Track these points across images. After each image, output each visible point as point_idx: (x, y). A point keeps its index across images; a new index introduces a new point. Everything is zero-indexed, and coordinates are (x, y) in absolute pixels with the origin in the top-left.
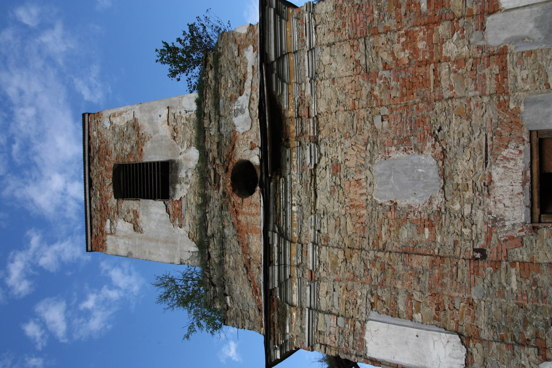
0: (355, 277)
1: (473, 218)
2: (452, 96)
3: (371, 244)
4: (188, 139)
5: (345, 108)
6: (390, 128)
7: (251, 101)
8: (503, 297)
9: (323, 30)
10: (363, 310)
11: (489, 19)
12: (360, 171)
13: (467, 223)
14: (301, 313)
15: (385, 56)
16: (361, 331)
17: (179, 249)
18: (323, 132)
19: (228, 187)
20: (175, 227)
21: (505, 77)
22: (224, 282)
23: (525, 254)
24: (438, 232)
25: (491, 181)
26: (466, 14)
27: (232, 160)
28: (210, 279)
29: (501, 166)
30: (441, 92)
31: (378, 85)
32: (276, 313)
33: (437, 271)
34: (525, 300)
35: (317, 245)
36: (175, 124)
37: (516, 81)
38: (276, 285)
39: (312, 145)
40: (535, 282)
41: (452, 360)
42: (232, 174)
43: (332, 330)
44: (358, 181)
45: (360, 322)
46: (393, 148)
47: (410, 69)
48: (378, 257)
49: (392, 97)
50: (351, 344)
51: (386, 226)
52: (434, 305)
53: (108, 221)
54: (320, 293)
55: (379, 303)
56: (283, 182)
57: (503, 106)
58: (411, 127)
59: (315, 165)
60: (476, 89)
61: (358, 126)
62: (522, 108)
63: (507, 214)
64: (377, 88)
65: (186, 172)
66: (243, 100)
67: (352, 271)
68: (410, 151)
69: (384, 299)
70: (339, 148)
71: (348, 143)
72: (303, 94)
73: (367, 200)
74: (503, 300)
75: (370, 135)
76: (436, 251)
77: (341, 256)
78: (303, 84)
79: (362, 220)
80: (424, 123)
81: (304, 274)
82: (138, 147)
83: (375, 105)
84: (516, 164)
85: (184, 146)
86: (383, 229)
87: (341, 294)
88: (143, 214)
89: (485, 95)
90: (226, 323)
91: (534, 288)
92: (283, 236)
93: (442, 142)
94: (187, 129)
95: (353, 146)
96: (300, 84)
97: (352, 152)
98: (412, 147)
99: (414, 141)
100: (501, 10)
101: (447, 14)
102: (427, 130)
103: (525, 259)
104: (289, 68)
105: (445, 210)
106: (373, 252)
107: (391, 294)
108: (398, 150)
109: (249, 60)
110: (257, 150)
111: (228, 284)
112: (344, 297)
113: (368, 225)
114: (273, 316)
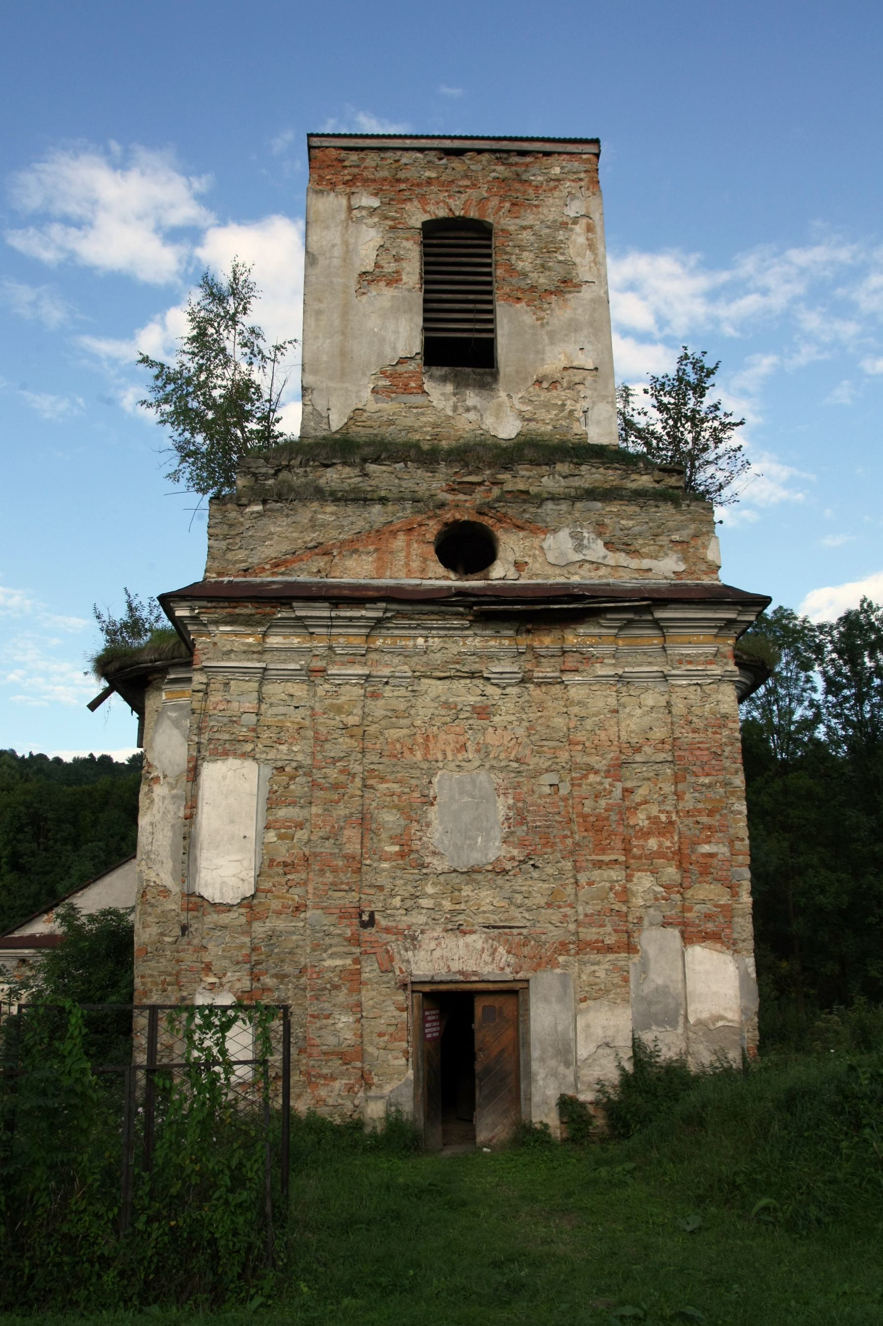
0: (321, 743)
2: (580, 884)
3: (372, 766)
4: (535, 414)
5: (572, 730)
7: (595, 565)
8: (313, 950)
9: (693, 697)
10: (272, 755)
11: (676, 932)
12: (478, 751)
13: (409, 903)
14: (254, 652)
15: (642, 792)
16: (239, 752)
17: (332, 385)
18: (538, 691)
19: (453, 515)
20: (373, 377)
21: (599, 951)
22: (286, 500)
23: (371, 975)
24: (394, 863)
25: (465, 933)
26: (686, 904)
27: (498, 525)
28: (287, 466)
29: (485, 945)
30: (585, 869)
31: (603, 780)
32: (253, 611)
33: (341, 863)
34: (311, 975)
35: (366, 681)
36: (565, 385)
37: (593, 964)
39: (520, 676)
40: (336, 987)
41: (218, 886)
42: (475, 523)
43: (235, 705)
44: (464, 747)
45: (253, 750)
46: (511, 801)
47: (621, 826)
48: (354, 777)
49: (584, 801)
50: (217, 736)
51: (399, 790)
52: (292, 859)
53: (375, 202)
54: (290, 684)
56: (462, 624)
57: (563, 949)
58: (540, 827)
59: (488, 679)
60: (586, 915)
61: (545, 749)
62: (558, 971)
63: (423, 953)
65: (475, 408)
66: (597, 550)
67: (329, 738)
68: (506, 825)
69: (292, 787)
70: (513, 718)
71: (521, 732)
72: (599, 660)
73: (437, 761)
74: (308, 950)
75: (531, 767)
76: (368, 862)
77: (352, 720)
78: (613, 661)
79: (407, 753)
80: (545, 845)
81: (319, 658)
82: (524, 291)
83: (574, 775)
84: (486, 963)
85: (523, 403)
86: (395, 786)
87: (292, 719)
89: (579, 926)
90: (214, 501)
91: (328, 986)
92: (379, 623)
93: (517, 870)
94: (554, 412)
95: (515, 740)
96: (614, 657)
97: (507, 738)
98: (512, 829)
99: (521, 831)
100: (685, 946)
101: (690, 880)
102: (535, 849)
103: (365, 976)
104: (641, 636)
105: (426, 874)
106: (361, 770)
107: (301, 798)
108: (509, 808)
109: (661, 563)
110: (513, 575)
111: (285, 508)
112: (289, 724)
113: (399, 763)
114: (247, 607)
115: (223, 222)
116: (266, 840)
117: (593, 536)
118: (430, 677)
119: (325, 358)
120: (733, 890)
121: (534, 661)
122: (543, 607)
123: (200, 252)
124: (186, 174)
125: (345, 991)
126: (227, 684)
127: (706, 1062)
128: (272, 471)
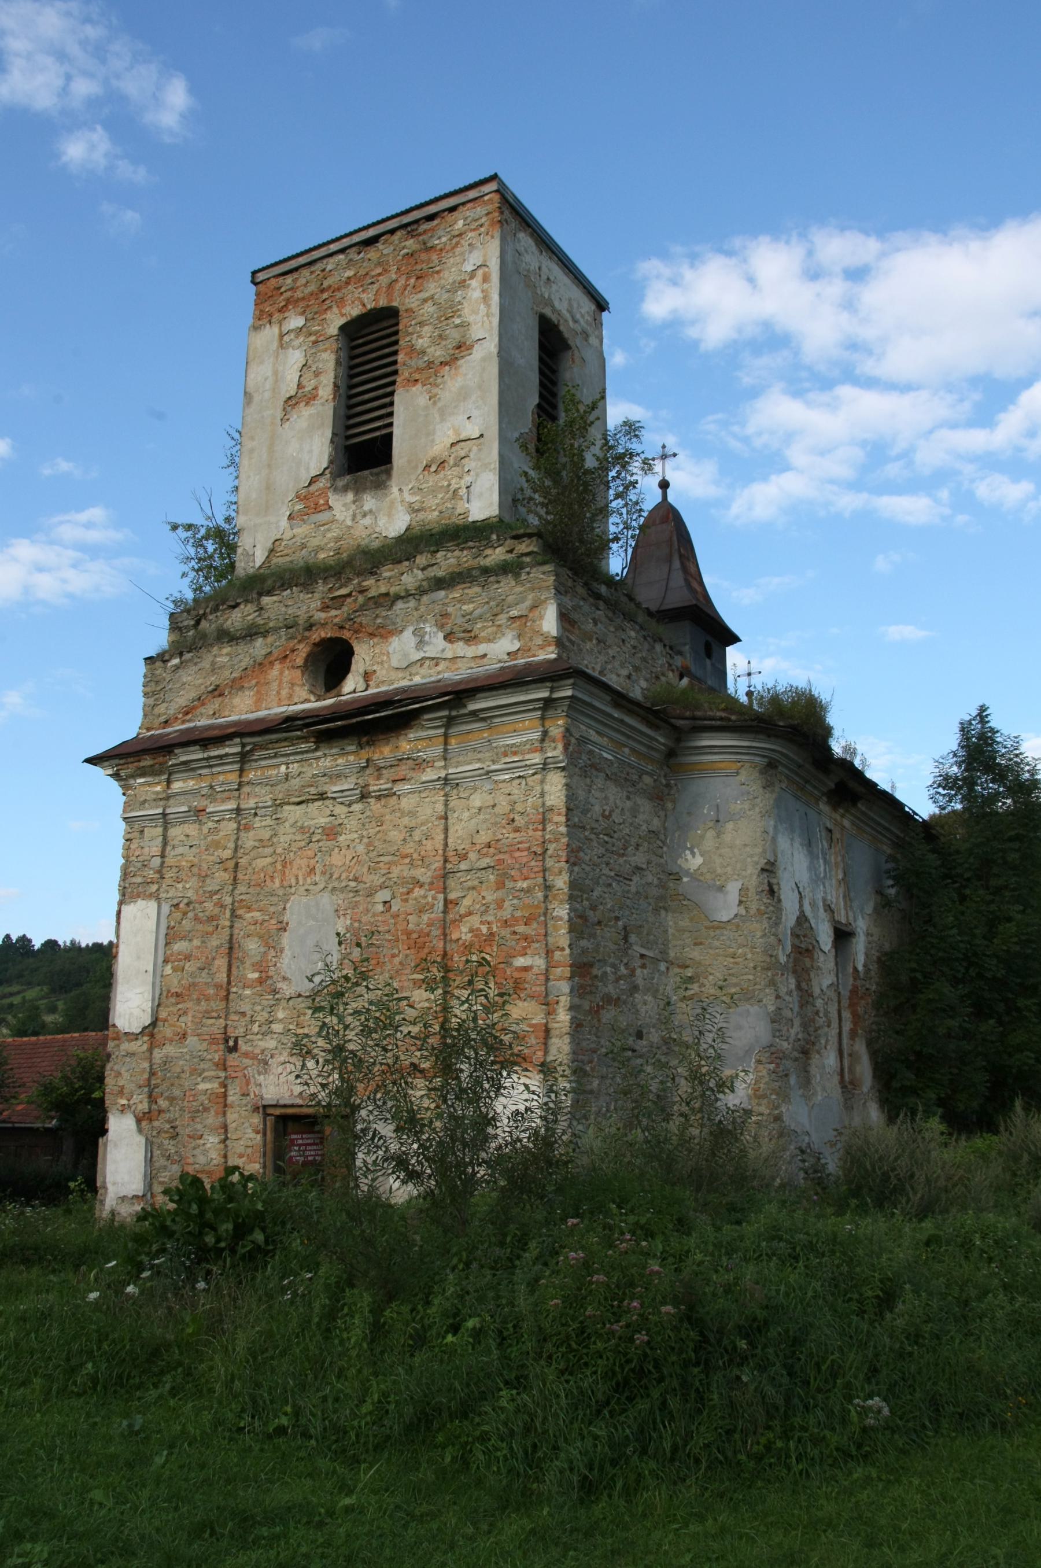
1: (270, 1035)
3: (242, 897)
6: (374, 915)
8: (191, 1074)
9: (516, 792)
13: (264, 1028)
14: (161, 799)
33: (212, 992)
38: (183, 759)
39: (358, 792)
40: (206, 1109)
41: (127, 1017)
43: (146, 850)
44: (312, 870)
45: (158, 890)
55: (178, 915)
59: (334, 798)
61: (381, 865)
63: (272, 1077)
66: (437, 645)
70: (355, 836)
71: (361, 849)
73: (291, 887)
86: (258, 914)
88: (310, 415)
92: (244, 758)
104: (470, 732)
112: (184, 863)
116: (165, 973)
117: (435, 629)
118: (289, 804)
119: (254, 496)
120: (549, 1005)
121: (376, 773)
122: (359, 719)
125: (213, 1112)
126: (142, 832)
127: (381, 1189)
128: (192, 623)
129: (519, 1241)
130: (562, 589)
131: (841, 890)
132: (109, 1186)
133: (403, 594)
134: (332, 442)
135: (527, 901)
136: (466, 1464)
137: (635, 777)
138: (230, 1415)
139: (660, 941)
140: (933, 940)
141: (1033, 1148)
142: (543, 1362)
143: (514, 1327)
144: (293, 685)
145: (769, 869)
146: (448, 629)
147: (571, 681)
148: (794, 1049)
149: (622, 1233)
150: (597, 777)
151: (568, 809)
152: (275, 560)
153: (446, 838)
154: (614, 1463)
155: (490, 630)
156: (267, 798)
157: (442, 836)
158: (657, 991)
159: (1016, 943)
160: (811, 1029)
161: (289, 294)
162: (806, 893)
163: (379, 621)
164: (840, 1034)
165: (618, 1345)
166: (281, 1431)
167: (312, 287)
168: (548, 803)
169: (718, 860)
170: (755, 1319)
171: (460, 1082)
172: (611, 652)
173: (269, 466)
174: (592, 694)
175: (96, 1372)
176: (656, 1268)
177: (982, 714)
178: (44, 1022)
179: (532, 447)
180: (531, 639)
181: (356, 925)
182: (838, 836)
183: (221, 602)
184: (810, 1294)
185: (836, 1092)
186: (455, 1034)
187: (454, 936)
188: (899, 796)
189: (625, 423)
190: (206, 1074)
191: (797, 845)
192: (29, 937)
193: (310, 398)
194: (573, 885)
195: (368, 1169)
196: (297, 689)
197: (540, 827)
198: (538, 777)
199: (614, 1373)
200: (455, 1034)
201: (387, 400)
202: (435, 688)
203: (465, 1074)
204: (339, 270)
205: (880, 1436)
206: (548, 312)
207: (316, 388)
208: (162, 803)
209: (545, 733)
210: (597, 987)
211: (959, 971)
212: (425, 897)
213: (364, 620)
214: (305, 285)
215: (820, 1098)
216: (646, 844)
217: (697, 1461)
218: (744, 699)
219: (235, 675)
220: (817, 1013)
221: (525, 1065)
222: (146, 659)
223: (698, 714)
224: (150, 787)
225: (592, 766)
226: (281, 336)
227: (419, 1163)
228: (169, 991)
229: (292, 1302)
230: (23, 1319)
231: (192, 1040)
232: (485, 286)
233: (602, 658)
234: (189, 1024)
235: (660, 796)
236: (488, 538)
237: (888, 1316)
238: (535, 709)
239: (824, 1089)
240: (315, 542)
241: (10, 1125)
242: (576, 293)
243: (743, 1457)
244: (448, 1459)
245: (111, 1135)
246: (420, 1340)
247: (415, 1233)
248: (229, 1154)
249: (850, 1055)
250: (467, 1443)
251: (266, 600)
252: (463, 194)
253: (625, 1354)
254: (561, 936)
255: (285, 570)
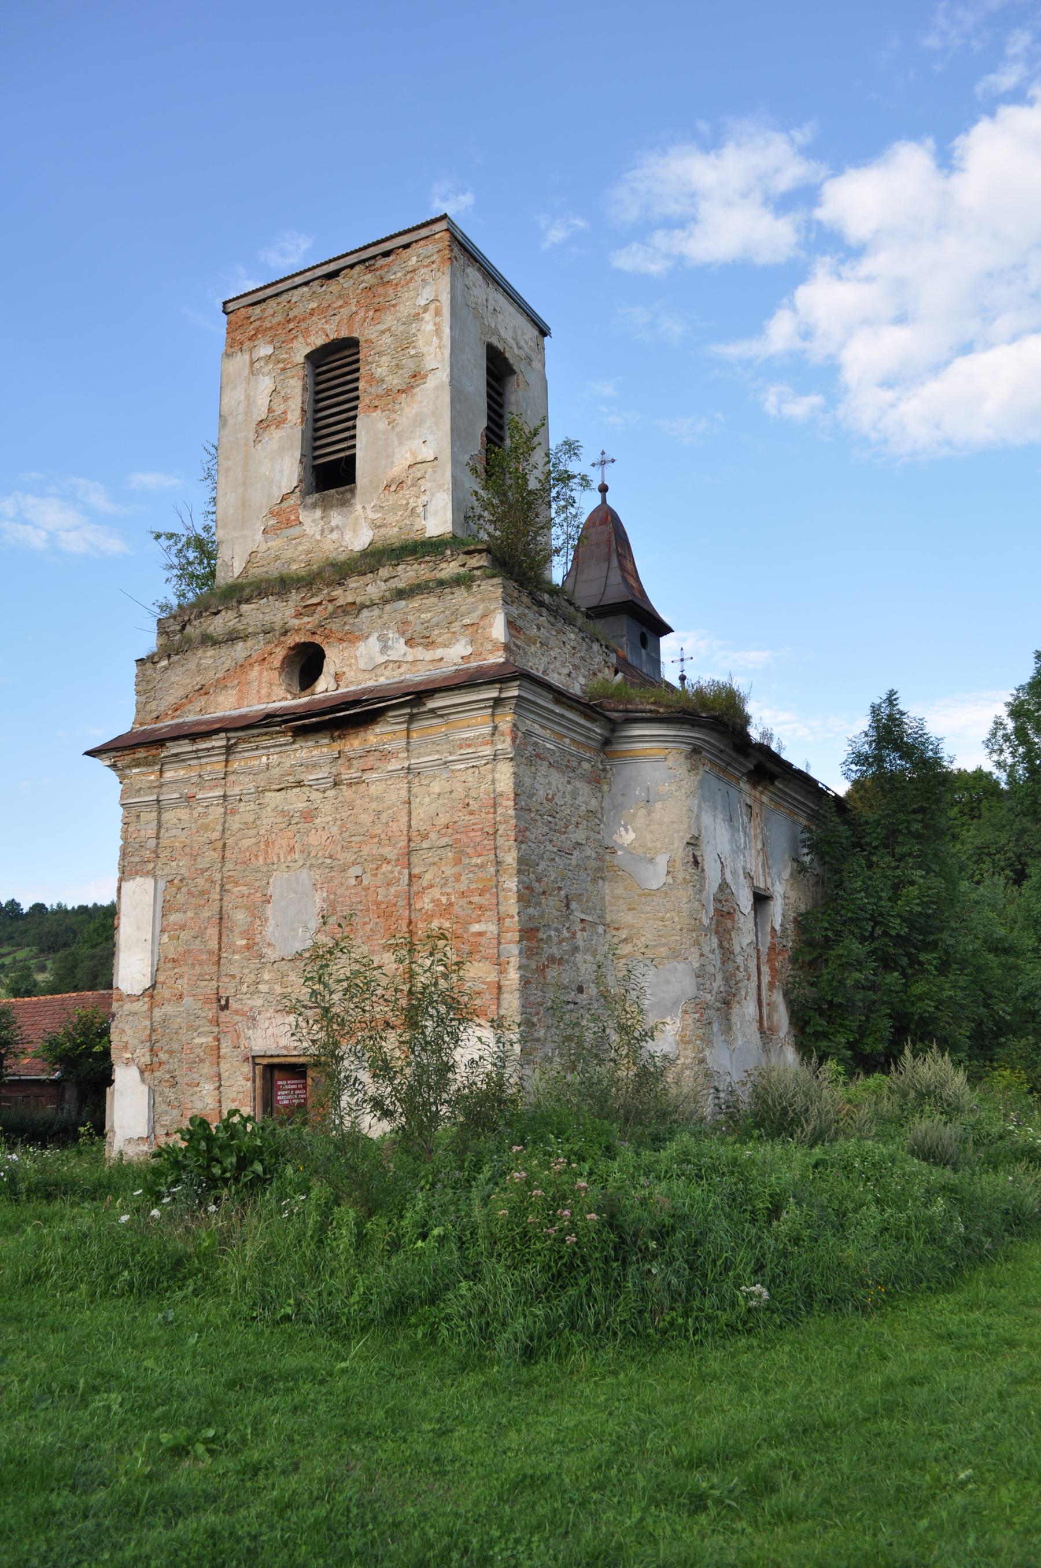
3: (230, 873)
8: (188, 1031)
9: (471, 779)
13: (252, 988)
32: (145, 755)
38: (174, 751)
39: (331, 780)
40: (202, 1061)
43: (143, 832)
44: (292, 849)
45: (154, 868)
59: (311, 786)
61: (353, 844)
64: (389, 868)
66: (399, 649)
70: (330, 818)
71: (335, 830)
86: (245, 888)
88: (280, 438)
112: (177, 844)
115: (838, 171)
117: (397, 636)
119: (231, 511)
120: (500, 965)
122: (331, 716)
123: (819, 214)
124: (785, 128)
125: (208, 1064)
128: (179, 628)
129: (475, 1166)
130: (509, 600)
131: (761, 858)
132: (116, 1129)
133: (368, 603)
134: (301, 462)
135: (481, 875)
136: (434, 1340)
137: (575, 764)
138: (245, 1308)
139: (598, 907)
140: (842, 903)
141: (919, 1086)
142: (494, 1260)
143: (471, 1233)
144: (271, 684)
145: (694, 843)
146: (408, 635)
147: (517, 683)
148: (716, 1001)
149: (558, 1157)
150: (541, 765)
151: (516, 795)
152: (252, 571)
153: (410, 820)
154: (550, 1336)
155: (445, 636)
156: (251, 785)
157: (406, 819)
158: (596, 950)
159: (918, 904)
160: (732, 983)
161: (258, 323)
162: (728, 863)
163: (347, 627)
164: (759, 987)
165: (552, 1245)
166: (287, 1318)
167: (279, 318)
168: (498, 790)
169: (649, 836)
170: (664, 1226)
171: (425, 1036)
172: (552, 653)
173: (244, 484)
174: (535, 693)
175: (132, 1278)
176: (584, 1184)
177: (891, 699)
178: (35, 981)
179: (480, 468)
180: (482, 645)
181: (332, 897)
182: (758, 811)
183: (203, 608)
184: (710, 1205)
185: (756, 1038)
186: (419, 996)
187: (418, 906)
188: (813, 774)
189: (565, 443)
190: (201, 1029)
191: (719, 820)
192: (17, 901)
193: (280, 422)
194: (521, 861)
195: (351, 1109)
196: (275, 688)
197: (492, 810)
198: (489, 766)
199: (550, 1267)
200: (419, 996)
201: (350, 424)
202: (398, 688)
203: (430, 1029)
204: (303, 300)
205: (761, 1315)
206: (494, 341)
207: (285, 412)
208: (155, 790)
209: (495, 728)
210: (543, 949)
211: (866, 930)
212: (392, 872)
213: (334, 627)
214: (273, 315)
215: (740, 1043)
216: (585, 822)
217: (615, 1334)
218: (677, 683)
219: (219, 675)
220: (738, 968)
221: (478, 1021)
222: (137, 661)
223: (630, 707)
224: (144, 776)
225: (537, 756)
226: (252, 363)
227: (393, 1103)
228: (166, 957)
229: (289, 1219)
230: (66, 1238)
231: (188, 1000)
232: (438, 319)
233: (545, 659)
234: (185, 986)
235: (597, 780)
236: (443, 553)
237: (775, 1223)
238: (486, 707)
239: (744, 1035)
240: (287, 555)
241: (17, 1078)
242: (522, 321)
243: (651, 1331)
244: (420, 1336)
245: (117, 1085)
246: (395, 1245)
247: (389, 1162)
248: (223, 1099)
249: (769, 1004)
250: (434, 1323)
251: (245, 608)
252: (416, 232)
253: (559, 1252)
254: (511, 905)
255: (261, 581)
